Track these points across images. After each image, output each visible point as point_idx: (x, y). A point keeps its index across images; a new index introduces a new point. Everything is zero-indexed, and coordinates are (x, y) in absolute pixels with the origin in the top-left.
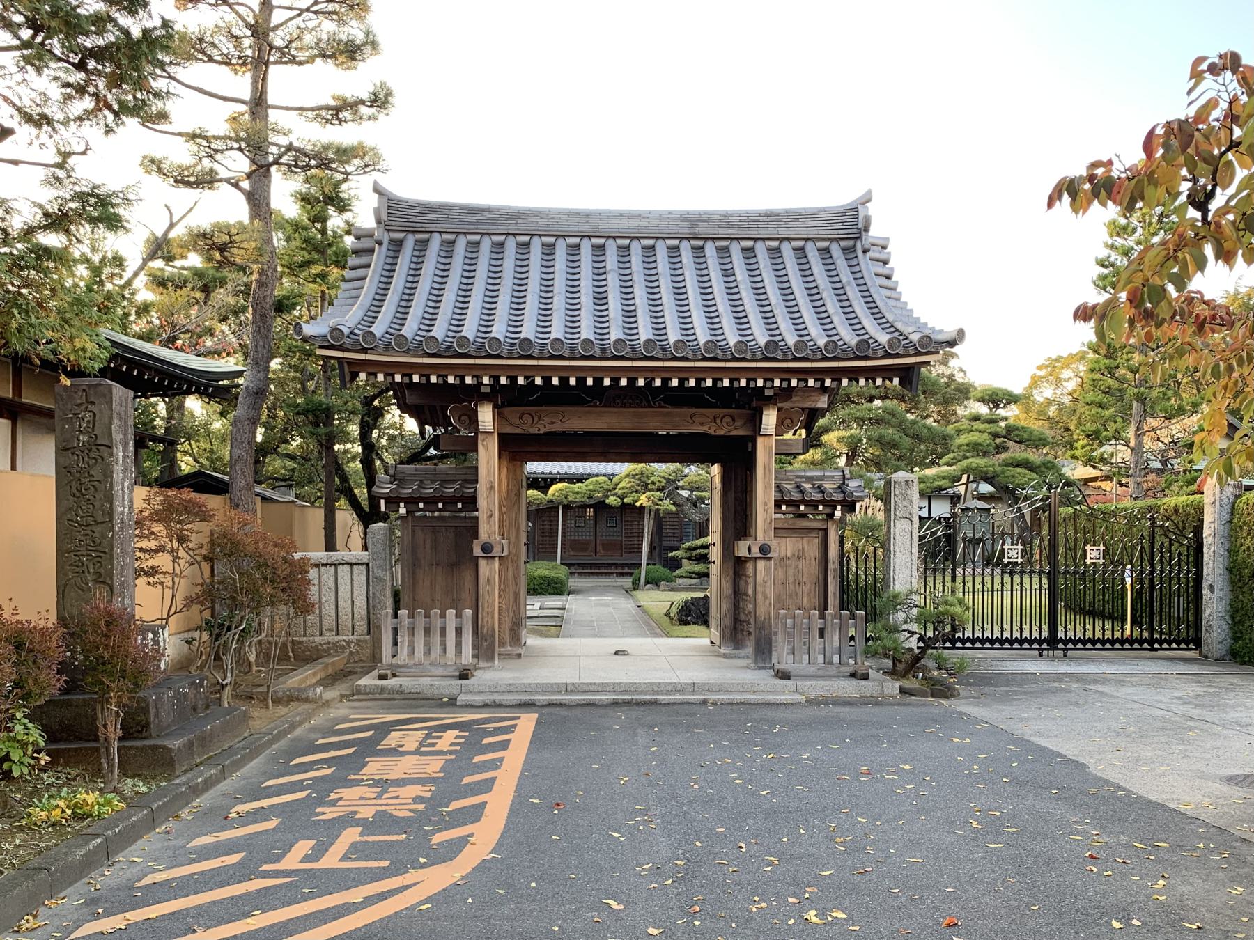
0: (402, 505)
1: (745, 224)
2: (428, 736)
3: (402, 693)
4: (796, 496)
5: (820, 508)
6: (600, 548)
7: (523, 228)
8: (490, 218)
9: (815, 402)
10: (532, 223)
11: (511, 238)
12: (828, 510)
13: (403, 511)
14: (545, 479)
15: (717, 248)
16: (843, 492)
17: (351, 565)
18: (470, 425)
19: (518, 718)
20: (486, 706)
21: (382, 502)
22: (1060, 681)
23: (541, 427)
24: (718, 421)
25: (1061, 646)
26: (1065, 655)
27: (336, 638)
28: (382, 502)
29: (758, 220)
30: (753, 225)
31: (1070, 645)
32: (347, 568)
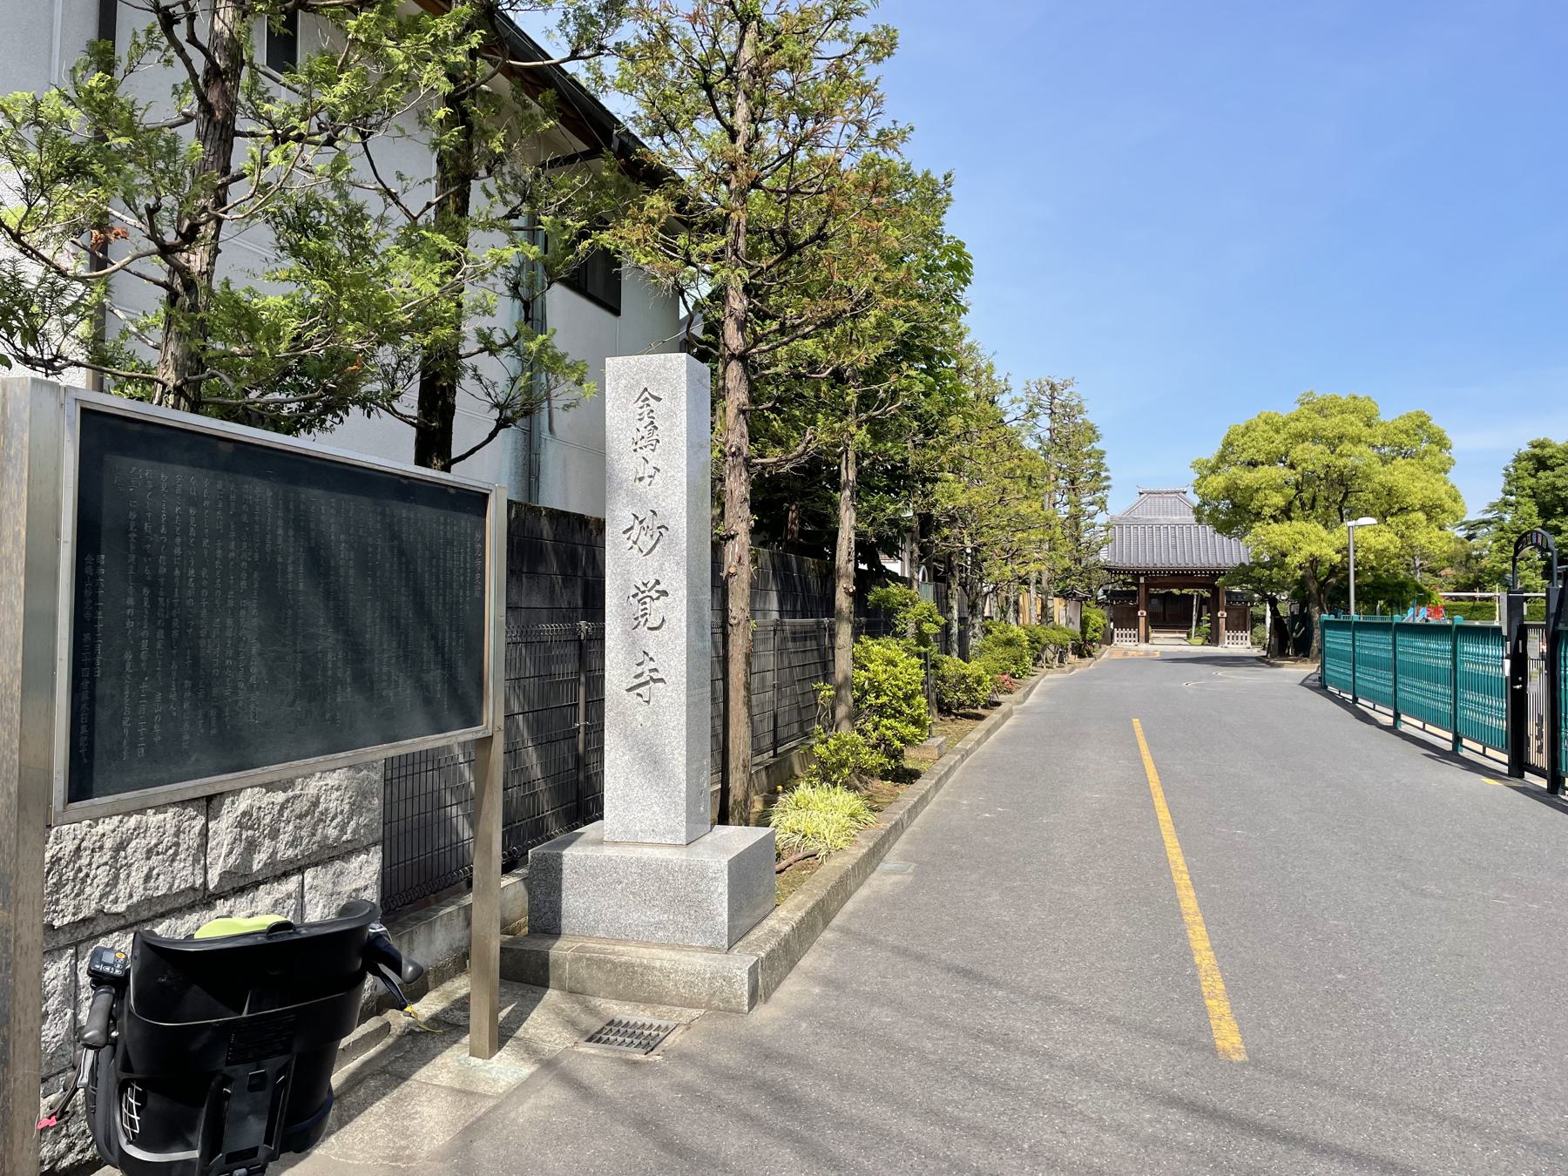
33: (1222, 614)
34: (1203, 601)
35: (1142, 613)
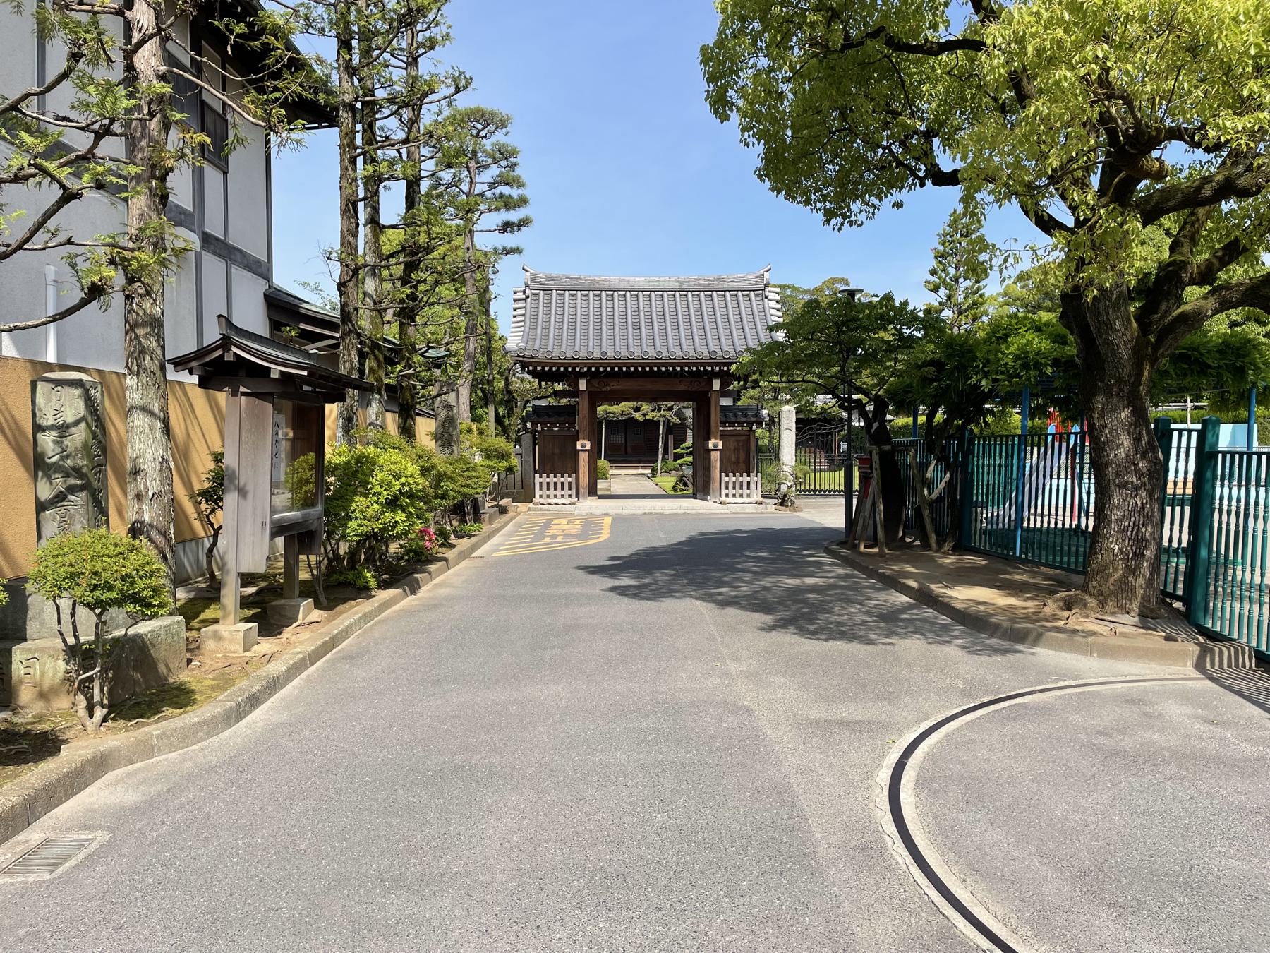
4: (733, 419)
6: (629, 449)
33: (715, 443)
34: (670, 428)
35: (583, 444)
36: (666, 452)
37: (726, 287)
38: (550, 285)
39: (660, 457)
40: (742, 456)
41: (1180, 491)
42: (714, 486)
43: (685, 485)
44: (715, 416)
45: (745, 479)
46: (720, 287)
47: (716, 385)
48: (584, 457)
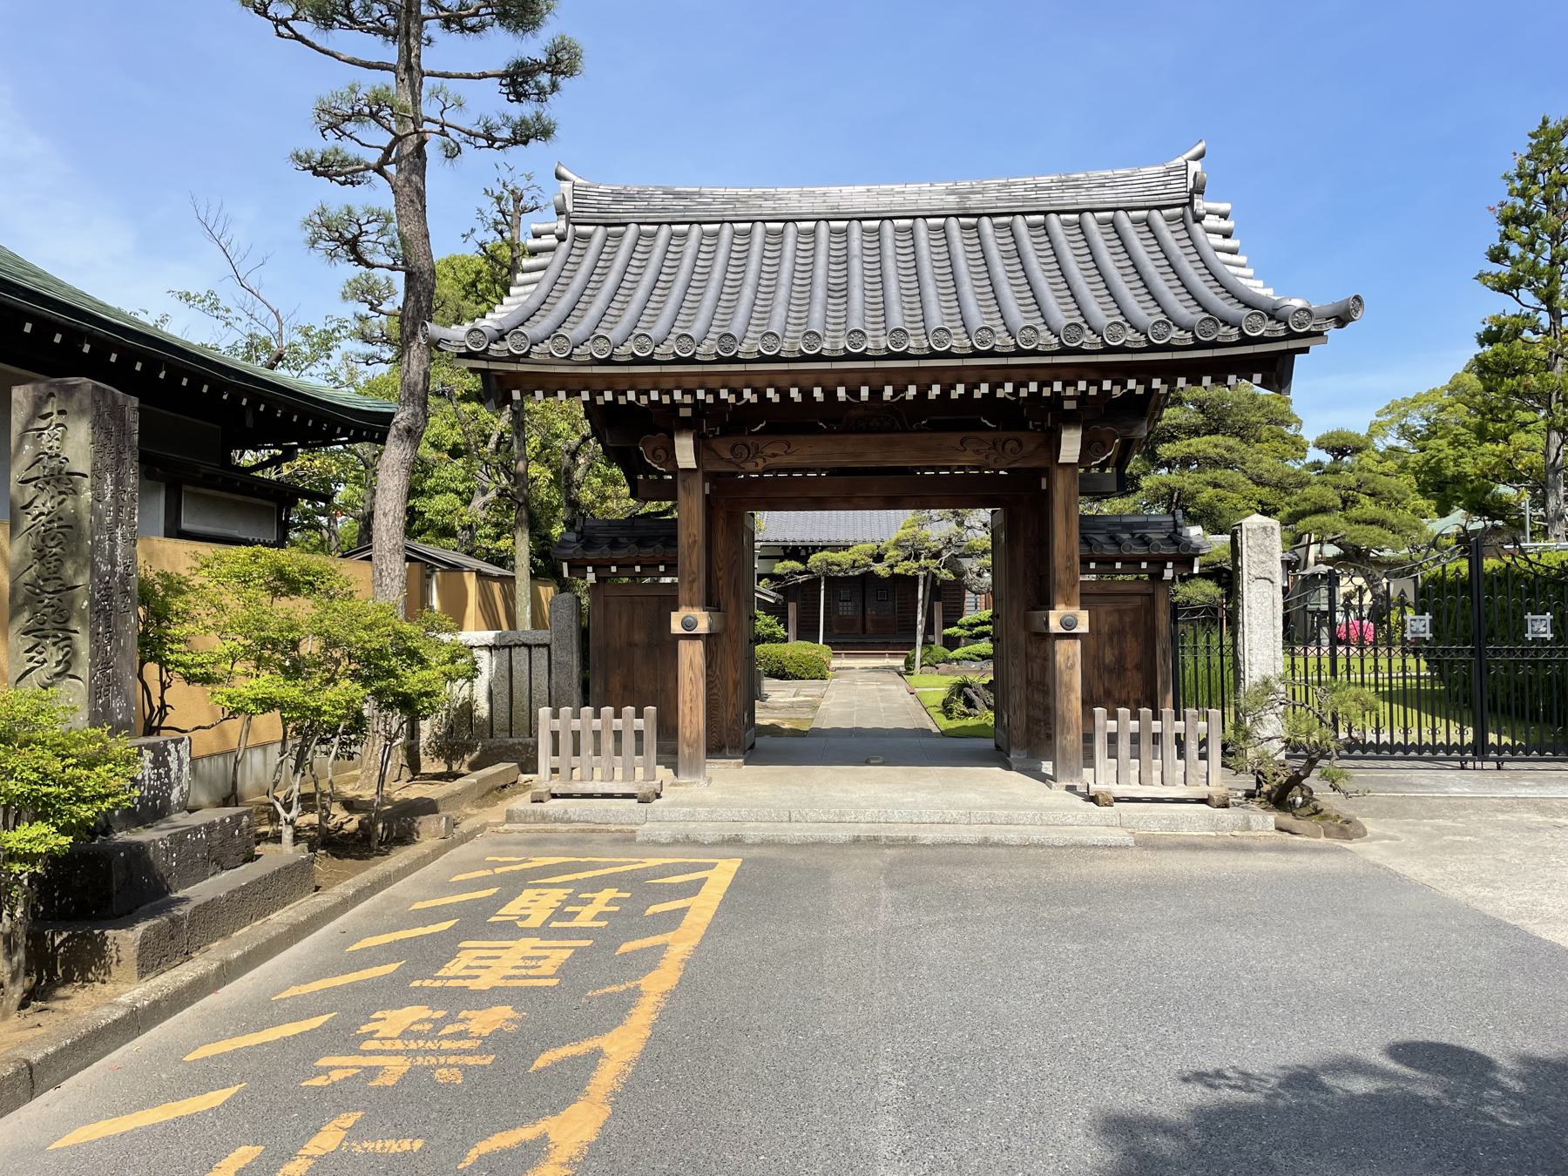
0: (590, 569)
1: (1033, 195)
2: (572, 900)
3: (569, 821)
4: (1110, 550)
5: (1144, 565)
6: (869, 625)
7: (742, 211)
8: (700, 203)
9: (1131, 428)
10: (754, 206)
11: (727, 225)
12: (1155, 569)
13: (591, 578)
14: (806, 548)
15: (994, 226)
16: (1176, 543)
17: (529, 647)
18: (667, 460)
19: (712, 866)
20: (675, 842)
21: (565, 565)
22: (1512, 809)
23: (760, 461)
24: (999, 447)
25: (1493, 755)
26: (1499, 768)
27: (511, 741)
28: (565, 565)
29: (1050, 188)
30: (1044, 194)
31: (1507, 754)
32: (525, 651)
33: (1067, 616)
36: (929, 629)
37: (1083, 200)
38: (622, 209)
39: (919, 639)
40: (1133, 648)
41: (1312, 650)
42: (1070, 739)
43: (969, 703)
44: (1064, 542)
45: (1169, 726)
46: (1069, 198)
47: (1070, 446)
48: (691, 657)
